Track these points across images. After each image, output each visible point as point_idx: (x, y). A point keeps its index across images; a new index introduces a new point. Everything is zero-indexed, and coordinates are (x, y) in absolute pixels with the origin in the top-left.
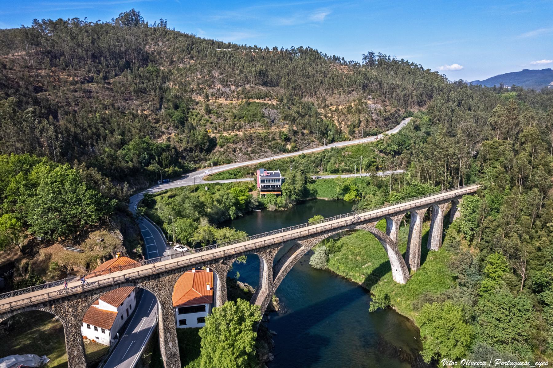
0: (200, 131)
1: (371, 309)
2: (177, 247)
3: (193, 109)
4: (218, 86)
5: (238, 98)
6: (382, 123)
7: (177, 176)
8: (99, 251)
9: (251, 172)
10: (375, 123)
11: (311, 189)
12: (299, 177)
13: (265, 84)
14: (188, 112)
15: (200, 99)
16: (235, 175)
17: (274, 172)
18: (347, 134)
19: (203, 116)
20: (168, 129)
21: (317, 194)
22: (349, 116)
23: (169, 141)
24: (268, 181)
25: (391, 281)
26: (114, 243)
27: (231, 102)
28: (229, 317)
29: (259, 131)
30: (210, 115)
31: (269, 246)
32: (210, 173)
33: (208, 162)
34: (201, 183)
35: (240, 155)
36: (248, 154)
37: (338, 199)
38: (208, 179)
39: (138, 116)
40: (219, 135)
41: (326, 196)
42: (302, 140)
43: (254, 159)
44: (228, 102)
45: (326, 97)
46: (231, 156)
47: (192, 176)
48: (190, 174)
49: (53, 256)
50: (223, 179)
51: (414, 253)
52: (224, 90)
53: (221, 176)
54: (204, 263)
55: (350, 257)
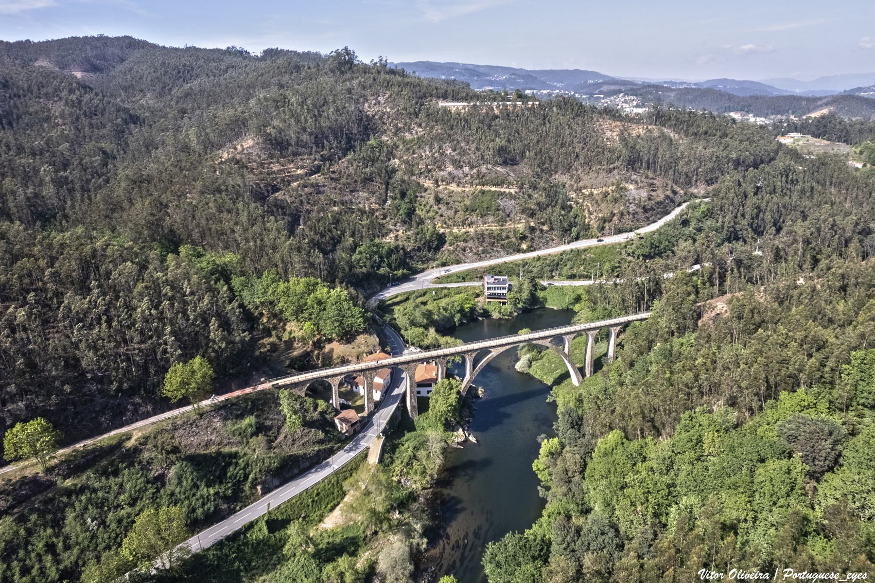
0: (428, 225)
1: (548, 401)
2: (412, 348)
3: (421, 197)
4: (450, 168)
5: (472, 184)
6: (641, 216)
7: (405, 279)
8: (363, 348)
9: (478, 275)
10: (631, 216)
12: (527, 286)
13: (505, 163)
14: (416, 202)
15: (428, 184)
16: (464, 278)
17: (501, 278)
18: (595, 231)
19: (431, 206)
20: (395, 225)
22: (603, 205)
23: (397, 240)
24: (495, 288)
25: (571, 383)
27: (463, 189)
28: (445, 386)
29: (491, 228)
30: (440, 206)
31: (470, 351)
32: (438, 275)
33: (436, 262)
34: (429, 287)
35: (470, 255)
36: (479, 254)
37: (568, 308)
38: (435, 283)
39: (365, 212)
40: (449, 230)
41: (556, 305)
42: (539, 238)
43: (485, 260)
44: (460, 189)
45: (582, 175)
46: (461, 255)
47: (420, 278)
48: (418, 276)
49: (335, 350)
50: (451, 282)
52: (455, 172)
53: (449, 280)
54: (432, 358)
55: (547, 364)
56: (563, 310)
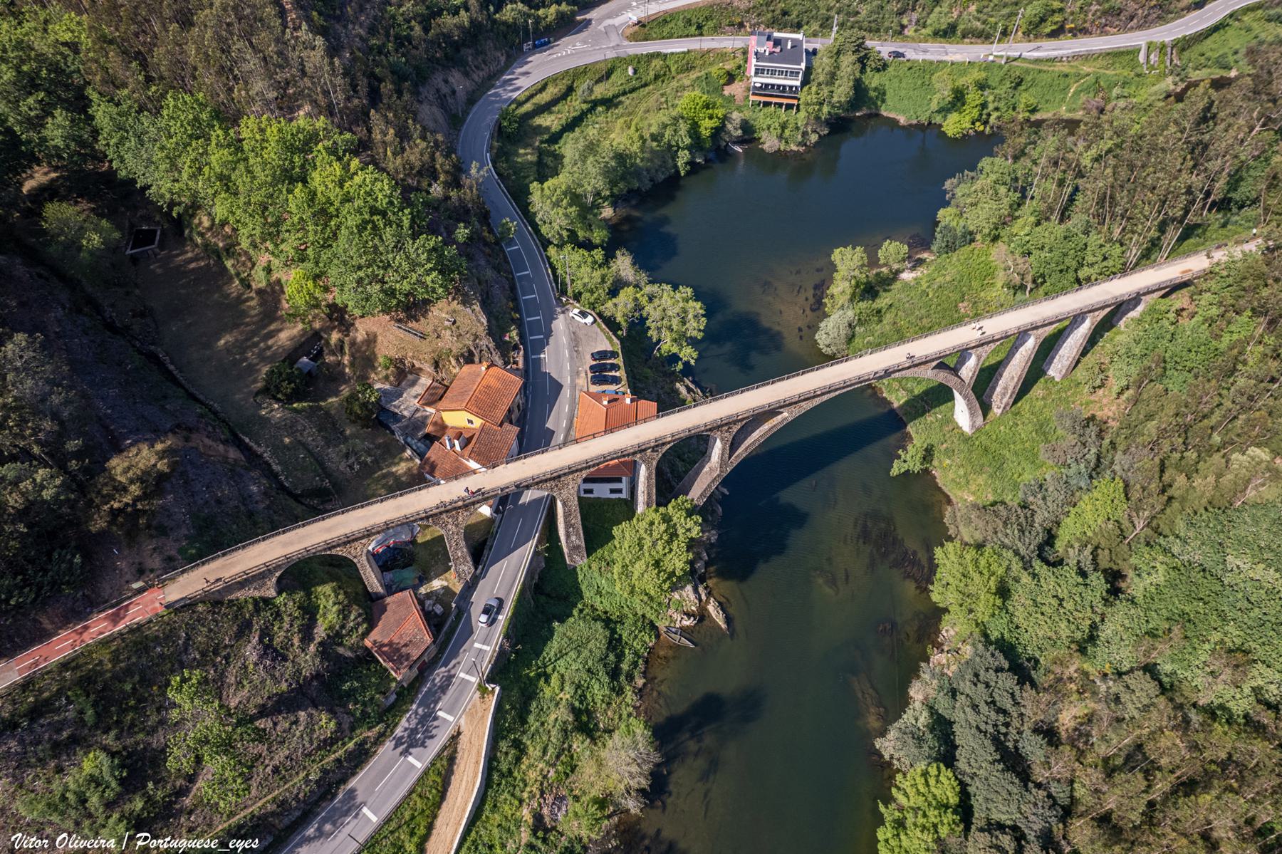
8: (449, 341)
11: (873, 85)
21: (883, 101)
25: (949, 420)
26: (473, 331)
41: (904, 112)
51: (1006, 388)
56: (919, 126)
